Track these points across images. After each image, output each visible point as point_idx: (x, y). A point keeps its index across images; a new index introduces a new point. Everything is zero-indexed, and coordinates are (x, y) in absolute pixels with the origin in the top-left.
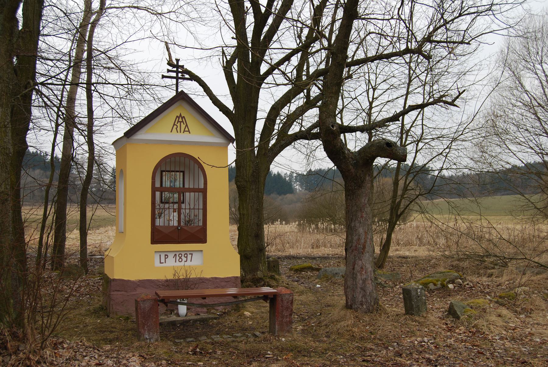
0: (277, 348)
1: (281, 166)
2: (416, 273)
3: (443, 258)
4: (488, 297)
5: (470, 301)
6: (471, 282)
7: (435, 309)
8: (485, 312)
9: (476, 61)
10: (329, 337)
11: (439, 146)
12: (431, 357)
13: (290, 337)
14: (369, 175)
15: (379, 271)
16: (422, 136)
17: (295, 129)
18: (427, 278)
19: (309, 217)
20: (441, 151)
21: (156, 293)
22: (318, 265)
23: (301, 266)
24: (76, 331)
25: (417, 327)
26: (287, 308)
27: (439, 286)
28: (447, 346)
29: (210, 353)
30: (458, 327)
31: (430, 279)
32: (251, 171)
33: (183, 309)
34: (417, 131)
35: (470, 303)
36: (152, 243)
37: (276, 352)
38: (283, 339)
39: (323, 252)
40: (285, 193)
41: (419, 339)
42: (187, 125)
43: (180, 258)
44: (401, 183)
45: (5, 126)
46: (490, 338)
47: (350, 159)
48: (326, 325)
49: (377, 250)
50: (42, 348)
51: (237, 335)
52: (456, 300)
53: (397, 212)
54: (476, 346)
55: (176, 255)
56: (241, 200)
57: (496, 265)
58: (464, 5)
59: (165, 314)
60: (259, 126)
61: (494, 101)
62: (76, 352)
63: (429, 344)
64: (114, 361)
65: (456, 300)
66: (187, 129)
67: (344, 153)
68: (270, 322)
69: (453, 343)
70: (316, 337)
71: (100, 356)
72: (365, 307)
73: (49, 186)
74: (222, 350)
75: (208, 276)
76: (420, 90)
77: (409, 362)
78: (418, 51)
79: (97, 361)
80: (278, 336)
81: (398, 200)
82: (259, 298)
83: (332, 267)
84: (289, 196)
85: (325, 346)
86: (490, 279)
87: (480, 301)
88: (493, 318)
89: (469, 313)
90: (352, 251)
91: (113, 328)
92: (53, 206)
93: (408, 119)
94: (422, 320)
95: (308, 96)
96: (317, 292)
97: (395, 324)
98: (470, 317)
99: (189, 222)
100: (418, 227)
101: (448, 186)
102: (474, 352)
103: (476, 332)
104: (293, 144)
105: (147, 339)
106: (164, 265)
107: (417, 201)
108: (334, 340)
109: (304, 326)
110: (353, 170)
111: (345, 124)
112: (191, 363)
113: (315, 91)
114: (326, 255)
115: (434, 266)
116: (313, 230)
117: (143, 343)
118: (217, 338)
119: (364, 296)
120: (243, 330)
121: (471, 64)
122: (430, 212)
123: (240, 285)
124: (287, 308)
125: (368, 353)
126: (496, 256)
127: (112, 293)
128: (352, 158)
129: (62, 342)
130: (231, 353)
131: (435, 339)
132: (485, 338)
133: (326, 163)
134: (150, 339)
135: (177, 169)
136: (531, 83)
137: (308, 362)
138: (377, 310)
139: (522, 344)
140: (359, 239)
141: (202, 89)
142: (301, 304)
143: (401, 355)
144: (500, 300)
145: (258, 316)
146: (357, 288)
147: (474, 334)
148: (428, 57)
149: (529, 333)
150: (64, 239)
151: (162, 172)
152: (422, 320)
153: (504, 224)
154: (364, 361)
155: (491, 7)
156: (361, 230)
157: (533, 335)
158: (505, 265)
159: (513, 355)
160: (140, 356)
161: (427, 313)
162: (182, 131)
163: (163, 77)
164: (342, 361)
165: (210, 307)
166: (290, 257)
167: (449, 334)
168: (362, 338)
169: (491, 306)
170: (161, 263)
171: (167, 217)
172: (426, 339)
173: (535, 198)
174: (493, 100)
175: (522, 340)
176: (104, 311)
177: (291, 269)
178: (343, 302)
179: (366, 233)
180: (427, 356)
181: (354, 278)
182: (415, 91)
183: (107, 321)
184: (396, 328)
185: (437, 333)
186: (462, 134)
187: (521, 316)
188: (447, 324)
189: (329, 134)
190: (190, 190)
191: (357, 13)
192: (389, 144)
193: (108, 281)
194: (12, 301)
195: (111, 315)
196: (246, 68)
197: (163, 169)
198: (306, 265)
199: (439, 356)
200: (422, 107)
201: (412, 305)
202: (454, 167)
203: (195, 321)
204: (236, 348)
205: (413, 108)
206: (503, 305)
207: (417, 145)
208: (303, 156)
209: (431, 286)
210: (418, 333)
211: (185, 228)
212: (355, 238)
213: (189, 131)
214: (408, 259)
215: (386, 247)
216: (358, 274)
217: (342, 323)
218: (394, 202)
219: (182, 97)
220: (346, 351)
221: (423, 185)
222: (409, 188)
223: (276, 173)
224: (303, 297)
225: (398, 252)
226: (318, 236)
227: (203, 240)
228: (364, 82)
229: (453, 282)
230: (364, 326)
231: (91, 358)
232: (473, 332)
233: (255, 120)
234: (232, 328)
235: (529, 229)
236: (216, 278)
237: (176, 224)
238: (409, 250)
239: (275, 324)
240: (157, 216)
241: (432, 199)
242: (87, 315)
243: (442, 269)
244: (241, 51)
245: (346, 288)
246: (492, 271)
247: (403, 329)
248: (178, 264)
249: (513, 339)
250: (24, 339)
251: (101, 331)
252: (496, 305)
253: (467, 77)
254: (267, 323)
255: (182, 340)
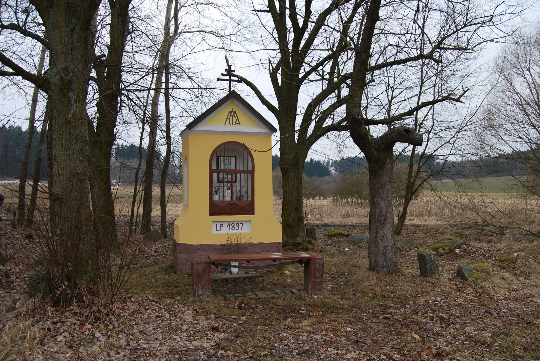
0: (310, 304)
1: (317, 153)
2: (427, 239)
3: (449, 227)
4: (490, 260)
5: (475, 265)
6: (474, 247)
7: (447, 269)
8: (489, 275)
9: (478, 65)
10: (355, 295)
11: (447, 135)
12: (444, 315)
13: (321, 295)
14: (390, 158)
15: (397, 238)
16: (432, 128)
17: (328, 122)
18: (437, 244)
19: (342, 193)
20: (448, 140)
21: (209, 257)
22: (347, 232)
23: (334, 233)
24: (148, 285)
25: (431, 288)
26: (319, 270)
27: (447, 250)
28: (457, 305)
29: (253, 308)
30: (466, 288)
31: (440, 245)
32: (292, 157)
33: (235, 270)
34: (428, 123)
35: (476, 266)
36: (210, 215)
37: (309, 308)
38: (316, 297)
39: (352, 221)
40: (323, 176)
41: (433, 298)
42: (238, 119)
43: (233, 227)
44: (415, 167)
45: (82, 119)
46: (495, 298)
47: (373, 144)
48: (352, 284)
49: (396, 219)
50: (112, 302)
51: (277, 291)
52: (464, 263)
53: (412, 190)
54: (483, 306)
55: (229, 224)
56: (284, 180)
57: (494, 233)
58: (468, 17)
59: (221, 272)
60: (299, 120)
61: (490, 101)
62: (140, 306)
63: (441, 303)
64: (171, 314)
65: (464, 263)
66: (237, 122)
67: (368, 139)
68: (304, 281)
69: (463, 303)
70: (344, 296)
71: (161, 309)
72: (385, 269)
73: (138, 170)
74: (263, 305)
75: (256, 242)
76: (431, 90)
77: (424, 320)
78: (430, 56)
79: (157, 314)
80: (311, 294)
81: (412, 180)
82: (295, 262)
83: (358, 234)
84: (327, 178)
85: (351, 303)
86: (490, 245)
87: (484, 265)
88: (497, 280)
89: (476, 276)
90: (375, 222)
91: (178, 283)
92: (141, 187)
93: (421, 114)
94: (435, 281)
95: (339, 96)
96: (346, 254)
97: (412, 284)
98: (476, 279)
99: (240, 197)
100: (427, 201)
101: (454, 168)
102: (482, 312)
103: (482, 293)
104: (326, 135)
105: (200, 295)
106: (220, 232)
107: (428, 180)
108: (359, 298)
109: (334, 284)
110: (377, 153)
111: (369, 117)
112: (235, 317)
113: (345, 92)
114: (354, 224)
115: (442, 234)
116: (344, 204)
117: (197, 298)
118: (261, 294)
119: (385, 260)
120: (282, 287)
121: (473, 68)
122: (439, 190)
123: (282, 249)
124: (319, 270)
125: (388, 311)
126: (493, 225)
127: (178, 255)
128: (375, 143)
129: (131, 297)
130: (271, 309)
131: (447, 298)
132: (491, 299)
133: (353, 151)
134: (203, 295)
135: (230, 155)
136: (521, 86)
137: (336, 319)
138: (396, 272)
139: (525, 304)
140: (381, 212)
141: (253, 92)
142: (332, 265)
143: (417, 313)
144: (501, 264)
145: (296, 275)
146: (379, 253)
147: (481, 294)
148: (438, 62)
149: (530, 295)
150: (150, 211)
151: (218, 157)
152: (435, 281)
153: (499, 199)
154: (384, 318)
155: (492, 18)
156: (383, 205)
157: (534, 296)
158: (502, 234)
159: (517, 315)
160: (194, 310)
161: (440, 275)
162: (234, 123)
163: (219, 79)
164: (365, 318)
165: (256, 268)
166: (325, 226)
167: (458, 293)
168: (383, 297)
169: (495, 269)
170: (217, 231)
171: (222, 194)
172: (438, 299)
173: (524, 178)
174: (489, 100)
175: (524, 300)
176: (172, 269)
177: (325, 235)
178: (367, 264)
179: (387, 207)
180: (440, 314)
181: (377, 245)
182: (427, 91)
183: (174, 277)
184: (413, 288)
185: (448, 293)
186: (466, 126)
187: (520, 278)
188: (456, 285)
189: (356, 126)
190: (241, 172)
191: (379, 17)
192: (407, 131)
193: (176, 245)
194: (90, 262)
195: (177, 272)
196: (288, 74)
197: (219, 155)
198: (337, 231)
199: (452, 315)
200: (433, 103)
201: (427, 269)
202: (460, 152)
203: (244, 278)
204: (275, 304)
205: (425, 105)
206: (504, 268)
207: (429, 135)
208: (335, 145)
209: (441, 251)
210: (432, 293)
211: (236, 202)
212: (378, 211)
213: (239, 123)
214: (421, 228)
215: (402, 218)
216: (380, 242)
217: (366, 283)
218: (409, 181)
219: (233, 96)
220: (369, 308)
221: (429, 169)
222: (421, 170)
223: (317, 161)
224: (332, 259)
225: (412, 222)
226: (348, 209)
227: (252, 213)
228: (384, 85)
229: (459, 247)
230: (385, 286)
231: (152, 311)
232: (479, 293)
233: (295, 115)
234: (274, 285)
235: (521, 203)
236: (262, 243)
237: (229, 199)
238: (420, 220)
239: (308, 284)
240: (214, 193)
241: (441, 179)
242: (159, 272)
243: (448, 236)
244: (283, 62)
245: (370, 253)
246: (491, 238)
247: (418, 289)
248: (231, 231)
249: (516, 300)
250: (96, 294)
251: (167, 286)
252: (498, 268)
253: (469, 78)
254: (302, 282)
255: (231, 296)
